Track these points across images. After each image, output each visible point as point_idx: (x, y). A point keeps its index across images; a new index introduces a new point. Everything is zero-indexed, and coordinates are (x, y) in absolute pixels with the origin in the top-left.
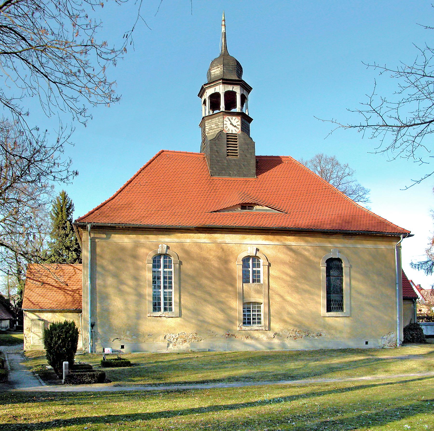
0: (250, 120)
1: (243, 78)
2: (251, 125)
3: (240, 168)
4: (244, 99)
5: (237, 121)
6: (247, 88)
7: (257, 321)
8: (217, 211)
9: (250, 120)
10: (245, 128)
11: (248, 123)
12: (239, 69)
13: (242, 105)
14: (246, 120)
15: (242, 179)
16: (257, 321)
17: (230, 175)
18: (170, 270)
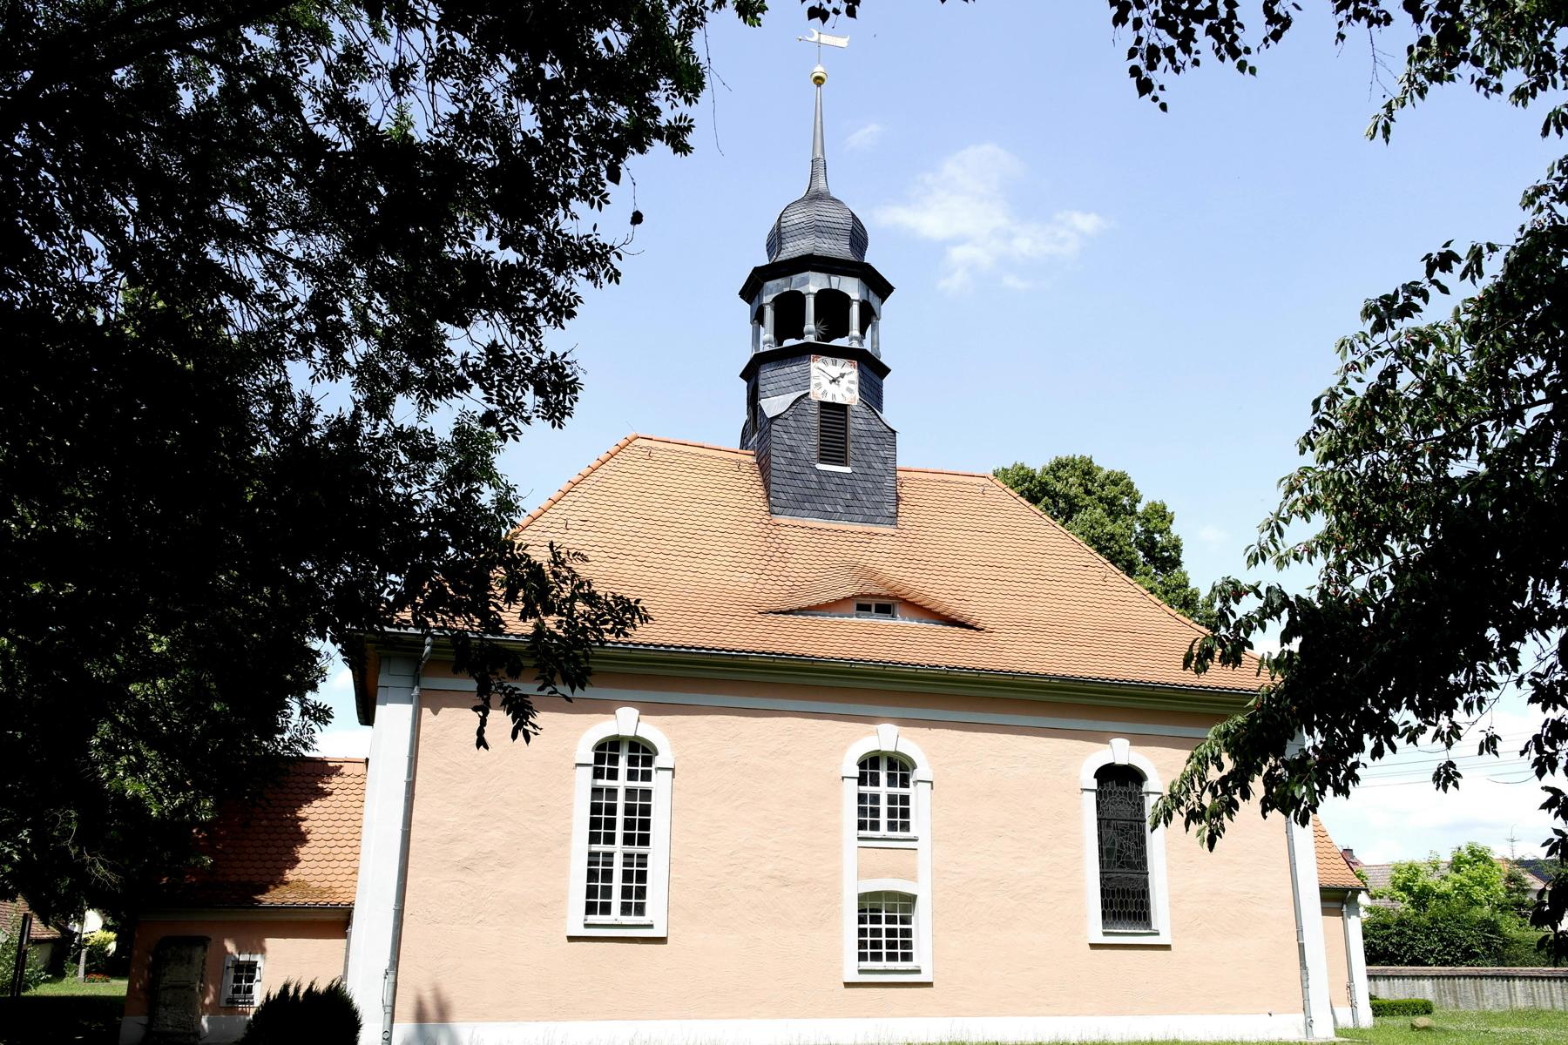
0: (884, 371)
1: (869, 258)
2: (887, 382)
3: (855, 496)
4: (868, 316)
5: (850, 373)
6: (879, 287)
7: (599, 900)
8: (791, 612)
9: (884, 371)
10: (872, 392)
11: (876, 378)
12: (858, 238)
13: (863, 331)
14: (872, 370)
15: (858, 527)
16: (640, 768)
17: (827, 515)
18: (632, 784)
